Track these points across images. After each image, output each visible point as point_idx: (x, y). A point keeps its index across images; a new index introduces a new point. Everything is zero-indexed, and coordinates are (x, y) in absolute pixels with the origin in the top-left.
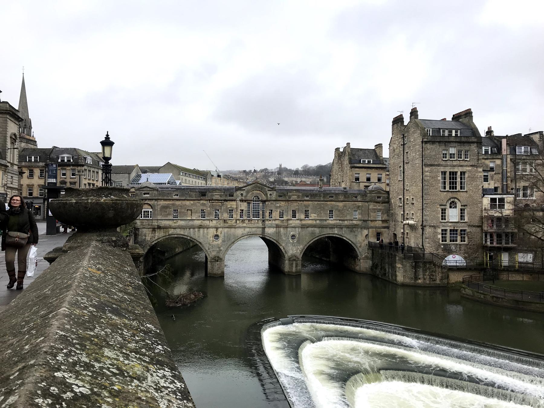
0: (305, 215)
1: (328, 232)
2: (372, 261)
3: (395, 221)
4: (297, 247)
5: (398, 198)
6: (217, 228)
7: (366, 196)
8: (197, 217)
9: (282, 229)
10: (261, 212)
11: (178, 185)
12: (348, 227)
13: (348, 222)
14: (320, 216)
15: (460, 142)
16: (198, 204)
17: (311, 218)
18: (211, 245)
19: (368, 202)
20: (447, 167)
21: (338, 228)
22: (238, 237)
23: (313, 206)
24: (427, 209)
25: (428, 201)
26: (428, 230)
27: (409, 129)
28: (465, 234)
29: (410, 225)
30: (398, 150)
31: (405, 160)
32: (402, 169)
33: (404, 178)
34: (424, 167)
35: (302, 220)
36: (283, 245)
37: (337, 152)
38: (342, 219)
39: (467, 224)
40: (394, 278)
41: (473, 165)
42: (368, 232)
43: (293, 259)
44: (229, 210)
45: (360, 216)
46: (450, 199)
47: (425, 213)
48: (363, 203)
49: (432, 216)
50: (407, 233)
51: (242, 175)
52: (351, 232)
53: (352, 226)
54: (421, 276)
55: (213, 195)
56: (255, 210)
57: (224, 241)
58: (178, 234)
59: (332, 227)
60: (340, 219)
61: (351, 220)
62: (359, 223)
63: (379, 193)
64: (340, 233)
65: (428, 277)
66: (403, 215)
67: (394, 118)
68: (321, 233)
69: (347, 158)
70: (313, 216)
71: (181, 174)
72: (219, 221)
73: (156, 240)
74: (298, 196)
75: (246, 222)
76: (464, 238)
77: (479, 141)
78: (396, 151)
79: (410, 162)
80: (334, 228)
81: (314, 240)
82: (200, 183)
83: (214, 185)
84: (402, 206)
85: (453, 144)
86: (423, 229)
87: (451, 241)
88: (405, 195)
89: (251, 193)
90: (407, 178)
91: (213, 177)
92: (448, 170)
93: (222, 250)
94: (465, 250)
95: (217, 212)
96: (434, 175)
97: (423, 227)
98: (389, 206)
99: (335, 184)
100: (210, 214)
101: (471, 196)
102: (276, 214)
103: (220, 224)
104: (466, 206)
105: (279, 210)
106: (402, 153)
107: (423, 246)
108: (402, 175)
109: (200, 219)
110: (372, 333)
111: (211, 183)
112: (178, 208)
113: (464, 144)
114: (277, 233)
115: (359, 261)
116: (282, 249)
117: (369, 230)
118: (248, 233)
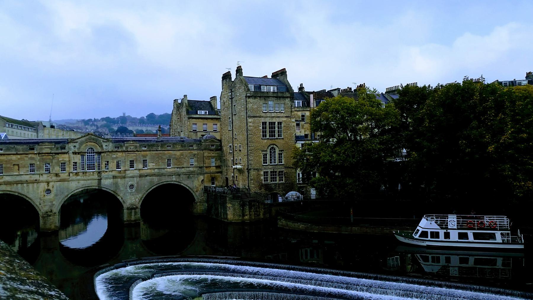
0: (143, 165)
1: (165, 180)
2: (208, 203)
3: (226, 166)
4: (135, 196)
5: (228, 146)
6: (48, 183)
7: (201, 145)
8: (25, 171)
9: (119, 180)
10: (96, 164)
11: (3, 138)
12: (185, 174)
13: (185, 169)
14: (159, 165)
15: (277, 96)
16: (25, 158)
17: (149, 168)
18: (42, 200)
19: (203, 150)
20: (267, 118)
21: (176, 175)
22: (72, 189)
23: (151, 156)
24: (252, 155)
25: (252, 147)
26: (252, 173)
27: (236, 84)
28: (282, 175)
29: (238, 169)
30: (227, 103)
31: (233, 112)
32: (231, 120)
33: (233, 128)
34: (248, 118)
35: (141, 170)
36: (121, 195)
37: (175, 103)
38: (179, 166)
39: (284, 166)
40: (225, 217)
41: (288, 116)
42: (204, 177)
43: (131, 209)
44: (61, 163)
45: (196, 163)
46: (270, 145)
47: (250, 159)
48: (198, 151)
49: (255, 161)
50: (237, 176)
51: (80, 125)
52: (188, 178)
53: (189, 172)
54: (247, 213)
55: (43, 148)
56: (90, 155)
57: (56, 195)
58: (4, 191)
59: (171, 175)
60: (177, 167)
61: (188, 168)
62: (195, 169)
63: (213, 141)
64: (178, 180)
65: (253, 213)
66: (233, 160)
67: (223, 75)
68: (159, 182)
69: (184, 109)
70: (151, 165)
71: (7, 125)
72: (50, 175)
73: (86, 187)
74: (136, 147)
75: (81, 174)
76: (282, 177)
77: (293, 96)
78: (226, 104)
79: (238, 114)
80: (172, 175)
81: (153, 188)
82: (30, 135)
83: (46, 137)
84: (231, 153)
85: (270, 99)
86: (248, 172)
87: (271, 181)
88: (234, 143)
89: (84, 145)
90: (235, 128)
91: (45, 128)
92: (268, 120)
93: (54, 204)
94: (283, 188)
95: (48, 165)
96: (256, 125)
97: (248, 170)
98: (222, 153)
99: (175, 134)
100: (40, 168)
101: (287, 143)
102: (112, 165)
103: (51, 178)
104: (283, 150)
105: (115, 161)
106: (231, 106)
107: (249, 187)
108: (231, 126)
109: (29, 174)
110: (250, 269)
111: (42, 135)
112: (3, 163)
113: (280, 98)
114: (114, 184)
115: (196, 204)
116: (120, 199)
117: (204, 176)
118: (83, 185)
